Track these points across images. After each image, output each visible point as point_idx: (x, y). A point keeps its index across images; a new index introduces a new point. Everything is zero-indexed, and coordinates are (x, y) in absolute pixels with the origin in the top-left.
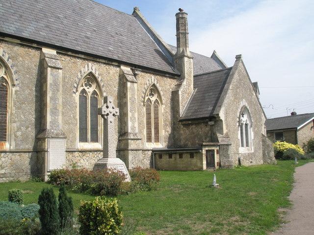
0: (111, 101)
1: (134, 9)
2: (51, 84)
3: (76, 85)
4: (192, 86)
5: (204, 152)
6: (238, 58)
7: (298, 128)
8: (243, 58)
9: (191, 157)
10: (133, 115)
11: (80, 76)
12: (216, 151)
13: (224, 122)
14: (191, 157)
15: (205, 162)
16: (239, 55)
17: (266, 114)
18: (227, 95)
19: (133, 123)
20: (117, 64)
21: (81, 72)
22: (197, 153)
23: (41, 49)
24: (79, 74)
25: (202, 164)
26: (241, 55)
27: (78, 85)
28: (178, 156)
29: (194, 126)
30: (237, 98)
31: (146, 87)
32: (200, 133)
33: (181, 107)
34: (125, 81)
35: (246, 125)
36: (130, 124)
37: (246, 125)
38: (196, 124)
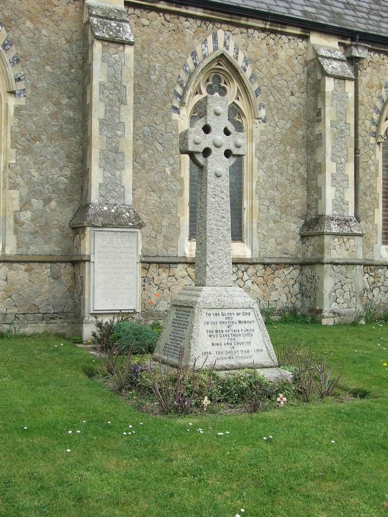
2: (102, 85)
11: (191, 67)
24: (190, 61)
34: (319, 77)
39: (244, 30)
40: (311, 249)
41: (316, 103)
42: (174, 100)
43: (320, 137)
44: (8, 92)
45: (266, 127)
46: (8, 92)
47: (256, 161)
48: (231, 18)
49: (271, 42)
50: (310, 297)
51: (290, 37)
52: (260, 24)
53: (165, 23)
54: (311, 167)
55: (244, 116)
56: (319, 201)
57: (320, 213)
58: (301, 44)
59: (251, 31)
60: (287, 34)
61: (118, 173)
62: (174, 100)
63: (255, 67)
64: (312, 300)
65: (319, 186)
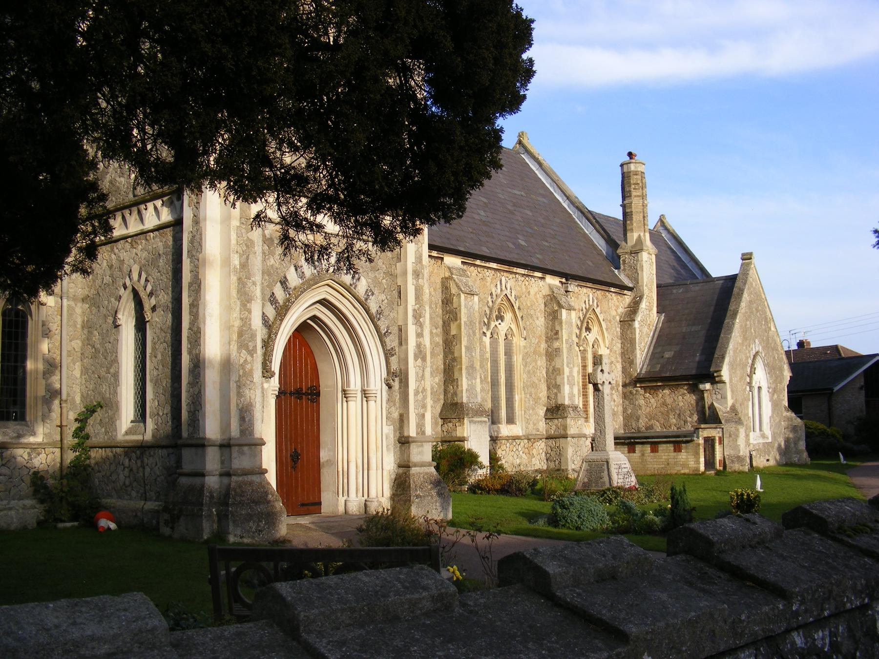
0: (607, 363)
1: (519, 136)
2: (465, 323)
3: (486, 321)
4: (655, 309)
5: (701, 441)
6: (747, 257)
7: (836, 389)
8: (755, 260)
9: (675, 451)
10: (571, 372)
11: (490, 304)
12: (717, 439)
13: (728, 385)
14: (675, 451)
15: (702, 460)
16: (747, 254)
17: (580, 274)
18: (733, 334)
19: (571, 387)
20: (539, 275)
21: (491, 294)
22: (687, 442)
23: (442, 259)
24: (490, 299)
25: (698, 462)
26: (751, 254)
27: (489, 319)
28: (648, 448)
29: (667, 391)
30: (746, 339)
31: (581, 315)
32: (681, 404)
33: (638, 352)
34: (556, 308)
35: (760, 388)
36: (465, 383)
37: (760, 388)
38: (670, 387)
39: (514, 276)
40: (554, 427)
41: (553, 326)
42: (484, 327)
43: (558, 351)
44: (127, 228)
45: (526, 343)
46: (127, 228)
47: (522, 367)
48: (509, 269)
49: (527, 283)
50: (555, 461)
51: (536, 279)
52: (494, 265)
53: (478, 274)
54: (551, 370)
55: (514, 336)
56: (558, 394)
57: (559, 403)
58: (541, 283)
59: (517, 276)
60: (475, 265)
61: (474, 381)
62: (484, 327)
63: (520, 302)
64: (557, 463)
65: (558, 384)
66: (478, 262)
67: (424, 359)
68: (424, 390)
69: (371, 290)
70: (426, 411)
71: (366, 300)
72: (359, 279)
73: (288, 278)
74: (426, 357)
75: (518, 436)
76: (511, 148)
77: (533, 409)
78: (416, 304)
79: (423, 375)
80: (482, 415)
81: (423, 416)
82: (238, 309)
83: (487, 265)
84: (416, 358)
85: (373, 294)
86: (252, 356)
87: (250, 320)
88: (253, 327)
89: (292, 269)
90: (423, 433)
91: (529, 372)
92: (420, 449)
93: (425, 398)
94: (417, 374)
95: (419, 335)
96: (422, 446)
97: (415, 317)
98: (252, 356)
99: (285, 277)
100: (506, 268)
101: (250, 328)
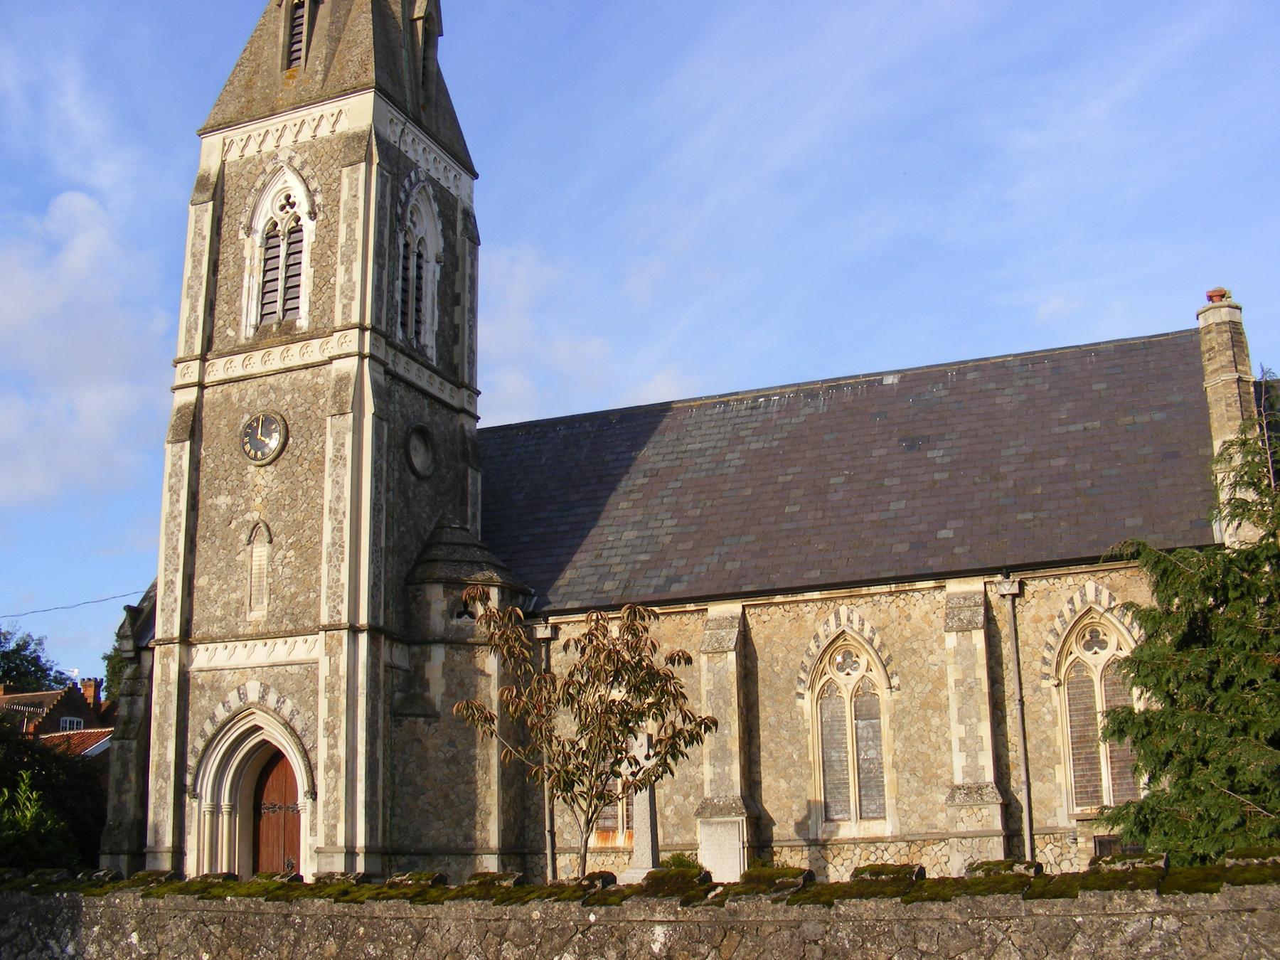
20: (931, 584)
66: (779, 599)
67: (338, 770)
68: (336, 800)
69: (297, 710)
70: (338, 822)
71: (291, 720)
72: (284, 702)
73: (217, 713)
74: (340, 768)
75: (878, 838)
76: (136, 605)
77: (920, 794)
78: (328, 717)
79: (335, 787)
80: (729, 814)
81: (335, 826)
82: (157, 747)
83: (800, 597)
84: (327, 770)
85: (298, 713)
86: (166, 783)
87: (166, 755)
88: (168, 760)
89: (220, 705)
90: (334, 844)
91: (907, 738)
92: (329, 860)
93: (337, 809)
94: (328, 786)
95: (332, 747)
96: (333, 856)
97: (327, 729)
98: (166, 783)
99: (214, 713)
100: (843, 592)
101: (165, 761)
